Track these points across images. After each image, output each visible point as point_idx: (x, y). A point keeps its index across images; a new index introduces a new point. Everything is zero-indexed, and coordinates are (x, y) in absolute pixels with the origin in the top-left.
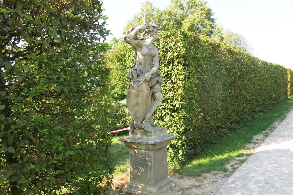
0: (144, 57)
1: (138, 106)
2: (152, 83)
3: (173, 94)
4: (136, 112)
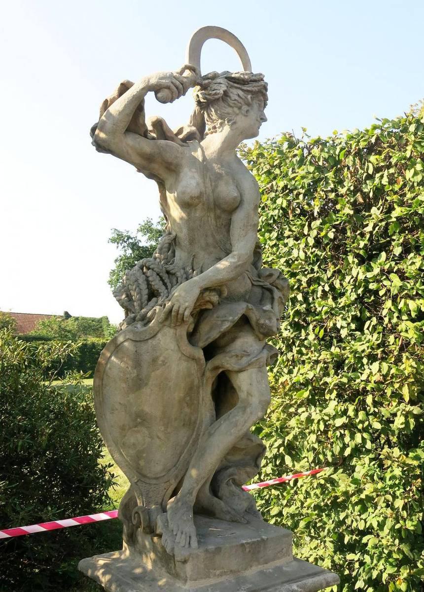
0: (189, 214)
1: (144, 430)
2: (211, 328)
3: (384, 372)
4: (138, 457)
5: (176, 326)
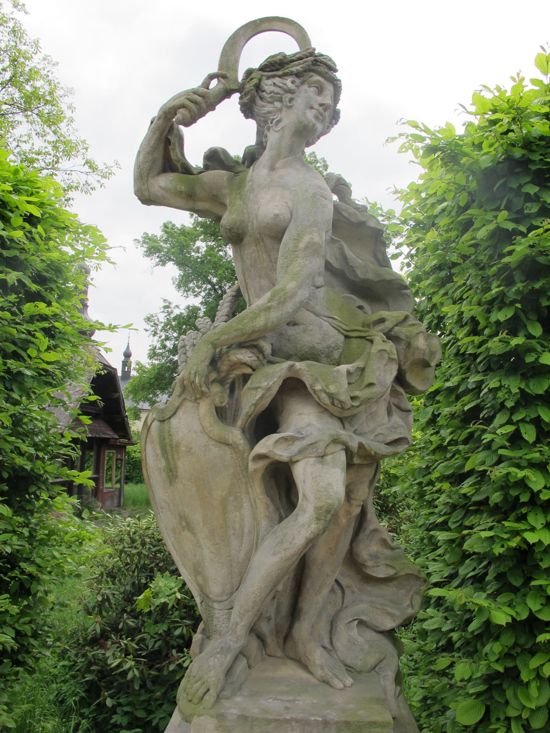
5: (196, 399)
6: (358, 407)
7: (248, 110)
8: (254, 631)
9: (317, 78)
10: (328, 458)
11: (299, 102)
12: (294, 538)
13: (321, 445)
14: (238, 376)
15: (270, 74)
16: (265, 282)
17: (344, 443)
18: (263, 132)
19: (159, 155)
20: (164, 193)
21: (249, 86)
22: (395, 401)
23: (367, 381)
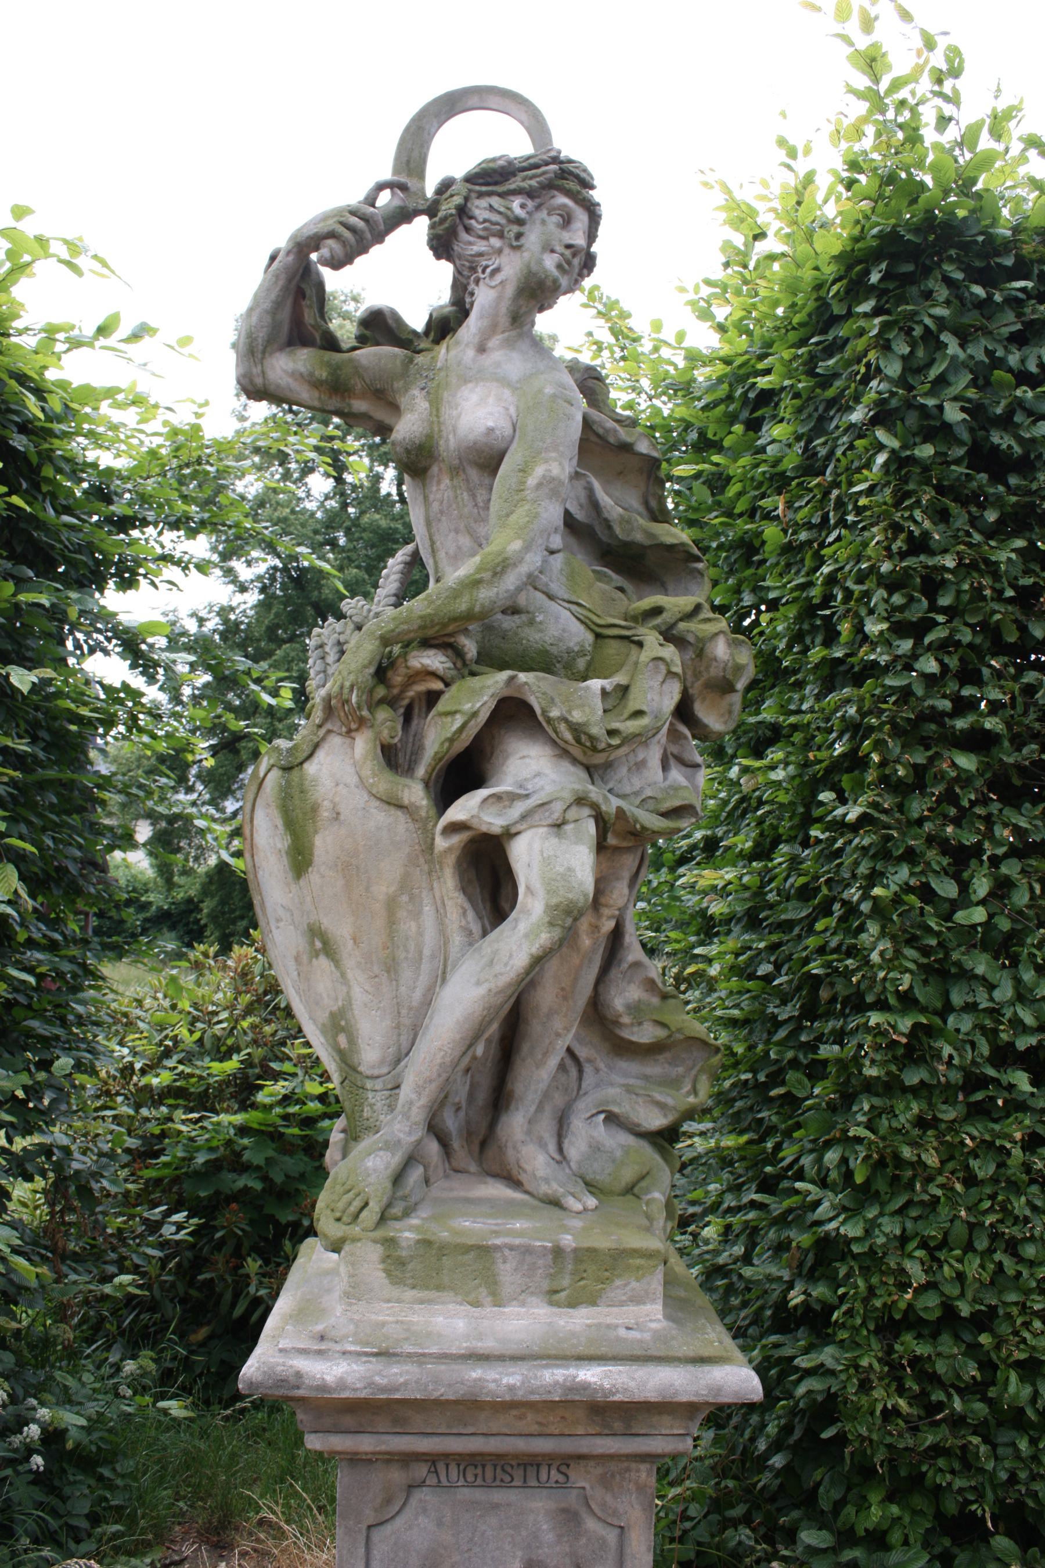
5: (350, 731)
6: (618, 747)
7: (442, 245)
8: (434, 1128)
9: (562, 200)
10: (569, 828)
11: (533, 238)
12: (511, 956)
13: (558, 808)
14: (419, 694)
15: (484, 189)
16: (465, 541)
17: (595, 806)
18: (465, 288)
19: (285, 315)
20: (290, 380)
21: (447, 208)
22: (674, 749)
23: (633, 705)
